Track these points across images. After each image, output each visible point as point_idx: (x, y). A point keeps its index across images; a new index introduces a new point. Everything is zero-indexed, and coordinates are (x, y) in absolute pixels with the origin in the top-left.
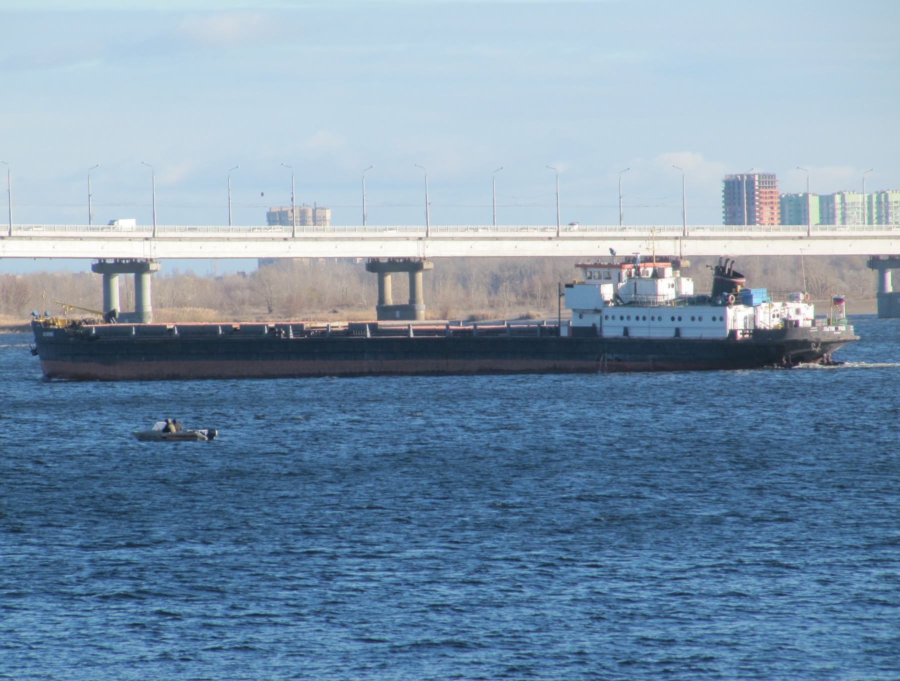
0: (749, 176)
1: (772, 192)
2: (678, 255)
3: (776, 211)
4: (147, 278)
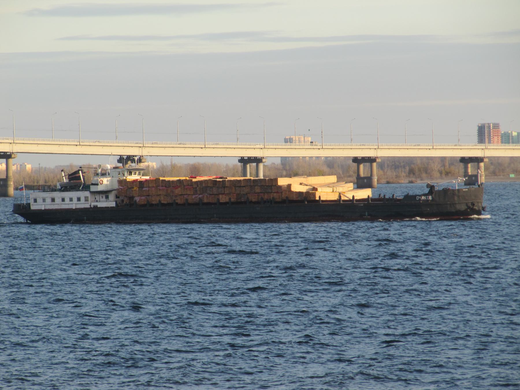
0: (488, 124)
2: (483, 156)
3: (500, 139)
4: (261, 166)
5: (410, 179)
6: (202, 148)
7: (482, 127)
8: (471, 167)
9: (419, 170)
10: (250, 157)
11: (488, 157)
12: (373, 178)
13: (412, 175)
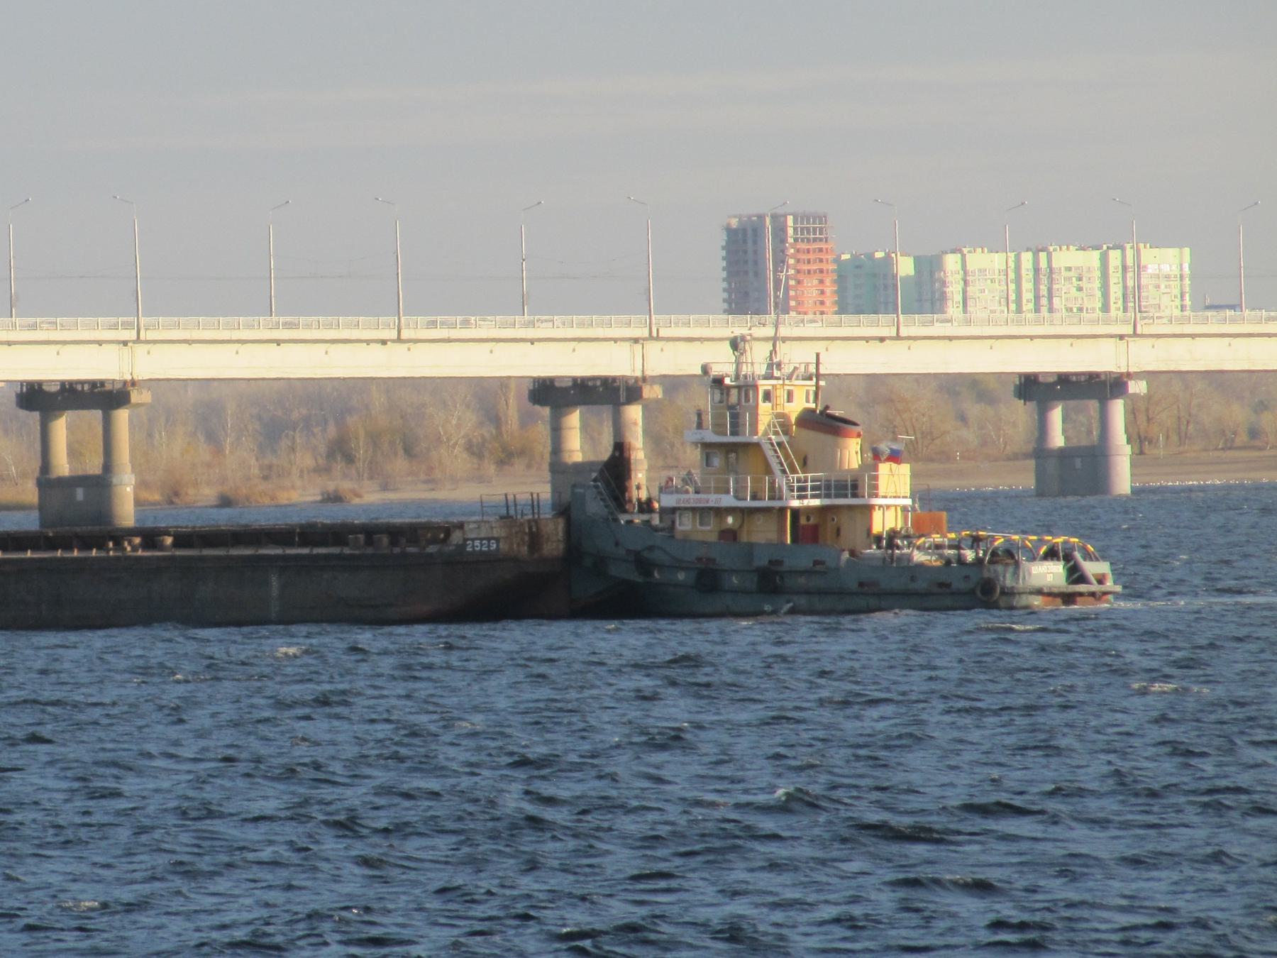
0: (775, 217)
1: (821, 250)
2: (638, 374)
3: (830, 288)
4: (1118, 409)
5: (331, 487)
6: (384, 342)
7: (744, 231)
8: (585, 427)
9: (374, 439)
10: (71, 383)
11: (153, 383)
12: (115, 481)
13: (339, 466)
